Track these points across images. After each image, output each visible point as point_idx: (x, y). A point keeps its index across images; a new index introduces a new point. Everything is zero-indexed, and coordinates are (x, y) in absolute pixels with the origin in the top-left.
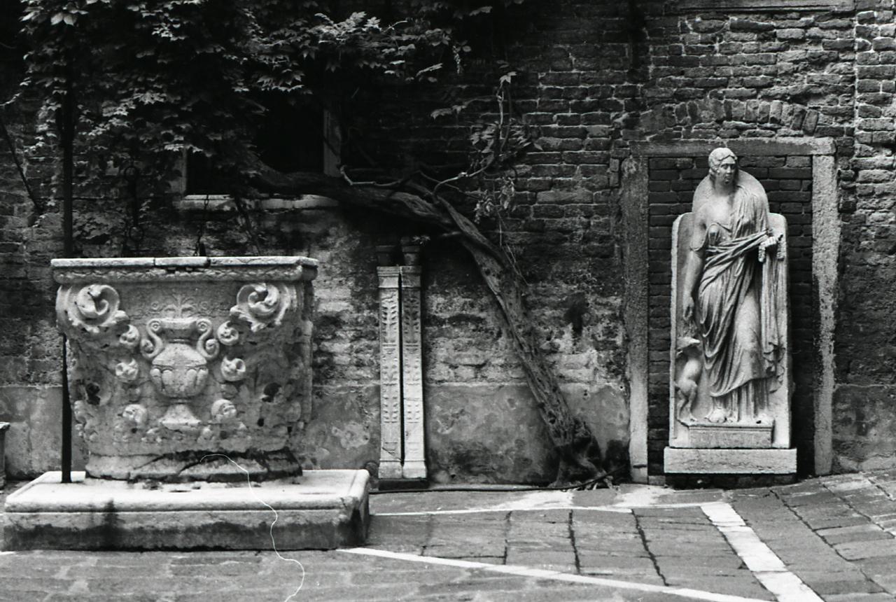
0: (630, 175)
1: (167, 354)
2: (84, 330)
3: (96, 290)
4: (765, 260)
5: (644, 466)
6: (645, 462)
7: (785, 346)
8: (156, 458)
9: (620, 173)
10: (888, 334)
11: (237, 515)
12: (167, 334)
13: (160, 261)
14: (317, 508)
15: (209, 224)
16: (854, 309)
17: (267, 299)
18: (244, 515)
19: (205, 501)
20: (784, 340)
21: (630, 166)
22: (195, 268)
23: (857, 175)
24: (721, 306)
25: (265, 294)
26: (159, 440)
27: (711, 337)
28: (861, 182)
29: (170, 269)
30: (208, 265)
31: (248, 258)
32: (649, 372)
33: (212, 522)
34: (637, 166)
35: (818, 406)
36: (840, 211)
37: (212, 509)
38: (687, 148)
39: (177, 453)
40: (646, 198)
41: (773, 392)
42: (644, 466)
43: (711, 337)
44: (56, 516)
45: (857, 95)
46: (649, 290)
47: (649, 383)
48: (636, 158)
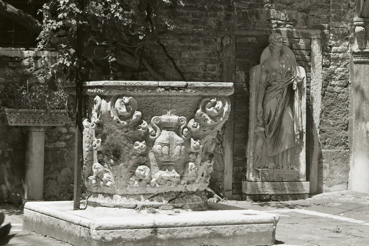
0: (227, 45)
1: (163, 136)
2: (118, 122)
3: (126, 100)
4: (296, 89)
5: (230, 190)
6: (231, 188)
7: (305, 131)
8: (137, 196)
9: (222, 44)
10: (343, 126)
11: (221, 228)
12: (164, 126)
13: (161, 83)
14: (262, 223)
15: (11, 64)
16: (329, 113)
17: (216, 106)
18: (225, 228)
19: (204, 221)
20: (304, 128)
21: (227, 41)
22: (179, 88)
23: (331, 49)
24: (276, 111)
25: (215, 104)
26: (157, 185)
27: (270, 128)
28: (333, 53)
29: (167, 88)
30: (186, 87)
31: (208, 83)
32: (233, 143)
33: (208, 232)
34: (230, 40)
35: (312, 161)
36: (323, 66)
37: (208, 225)
38: (254, 32)
39: (165, 193)
40: (234, 57)
41: (297, 154)
42: (230, 190)
43: (270, 128)
44: (124, 231)
45: (332, 10)
46: (235, 103)
47: (234, 149)
48: (230, 36)
